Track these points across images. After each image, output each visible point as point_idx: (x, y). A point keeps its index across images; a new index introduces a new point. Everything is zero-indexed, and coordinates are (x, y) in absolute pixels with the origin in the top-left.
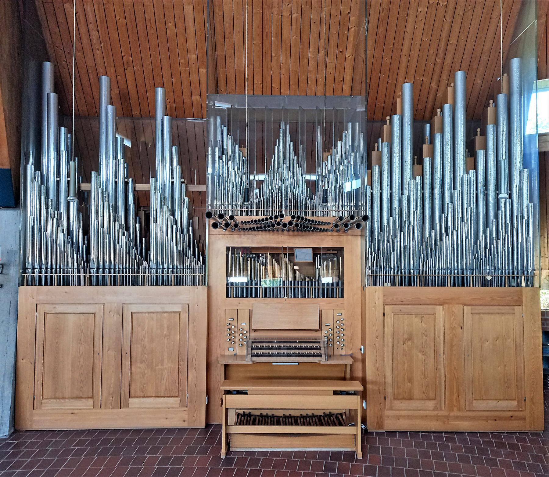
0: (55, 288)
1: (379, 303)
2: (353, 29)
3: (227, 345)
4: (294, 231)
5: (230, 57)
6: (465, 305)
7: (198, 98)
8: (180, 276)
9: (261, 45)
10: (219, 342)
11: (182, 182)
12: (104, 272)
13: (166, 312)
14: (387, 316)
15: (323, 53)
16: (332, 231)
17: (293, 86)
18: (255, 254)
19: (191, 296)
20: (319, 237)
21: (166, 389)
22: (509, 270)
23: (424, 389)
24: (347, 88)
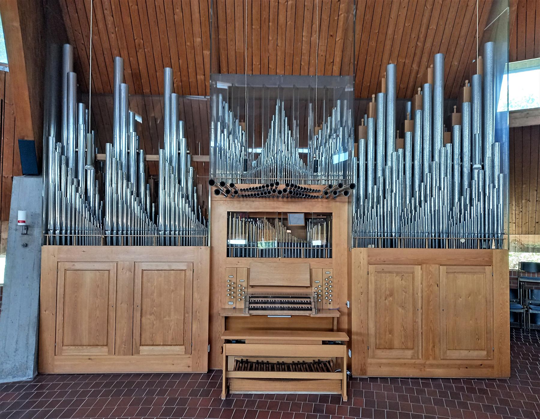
0: (121, 248)
2: (342, 15)
4: (288, 197)
5: (231, 40)
6: (441, 265)
7: (202, 77)
13: (173, 270)
15: (315, 36)
16: (322, 197)
17: (288, 67)
18: (253, 218)
19: (196, 255)
20: (311, 203)
21: (173, 339)
22: (481, 233)
23: (403, 340)
24: (336, 69)
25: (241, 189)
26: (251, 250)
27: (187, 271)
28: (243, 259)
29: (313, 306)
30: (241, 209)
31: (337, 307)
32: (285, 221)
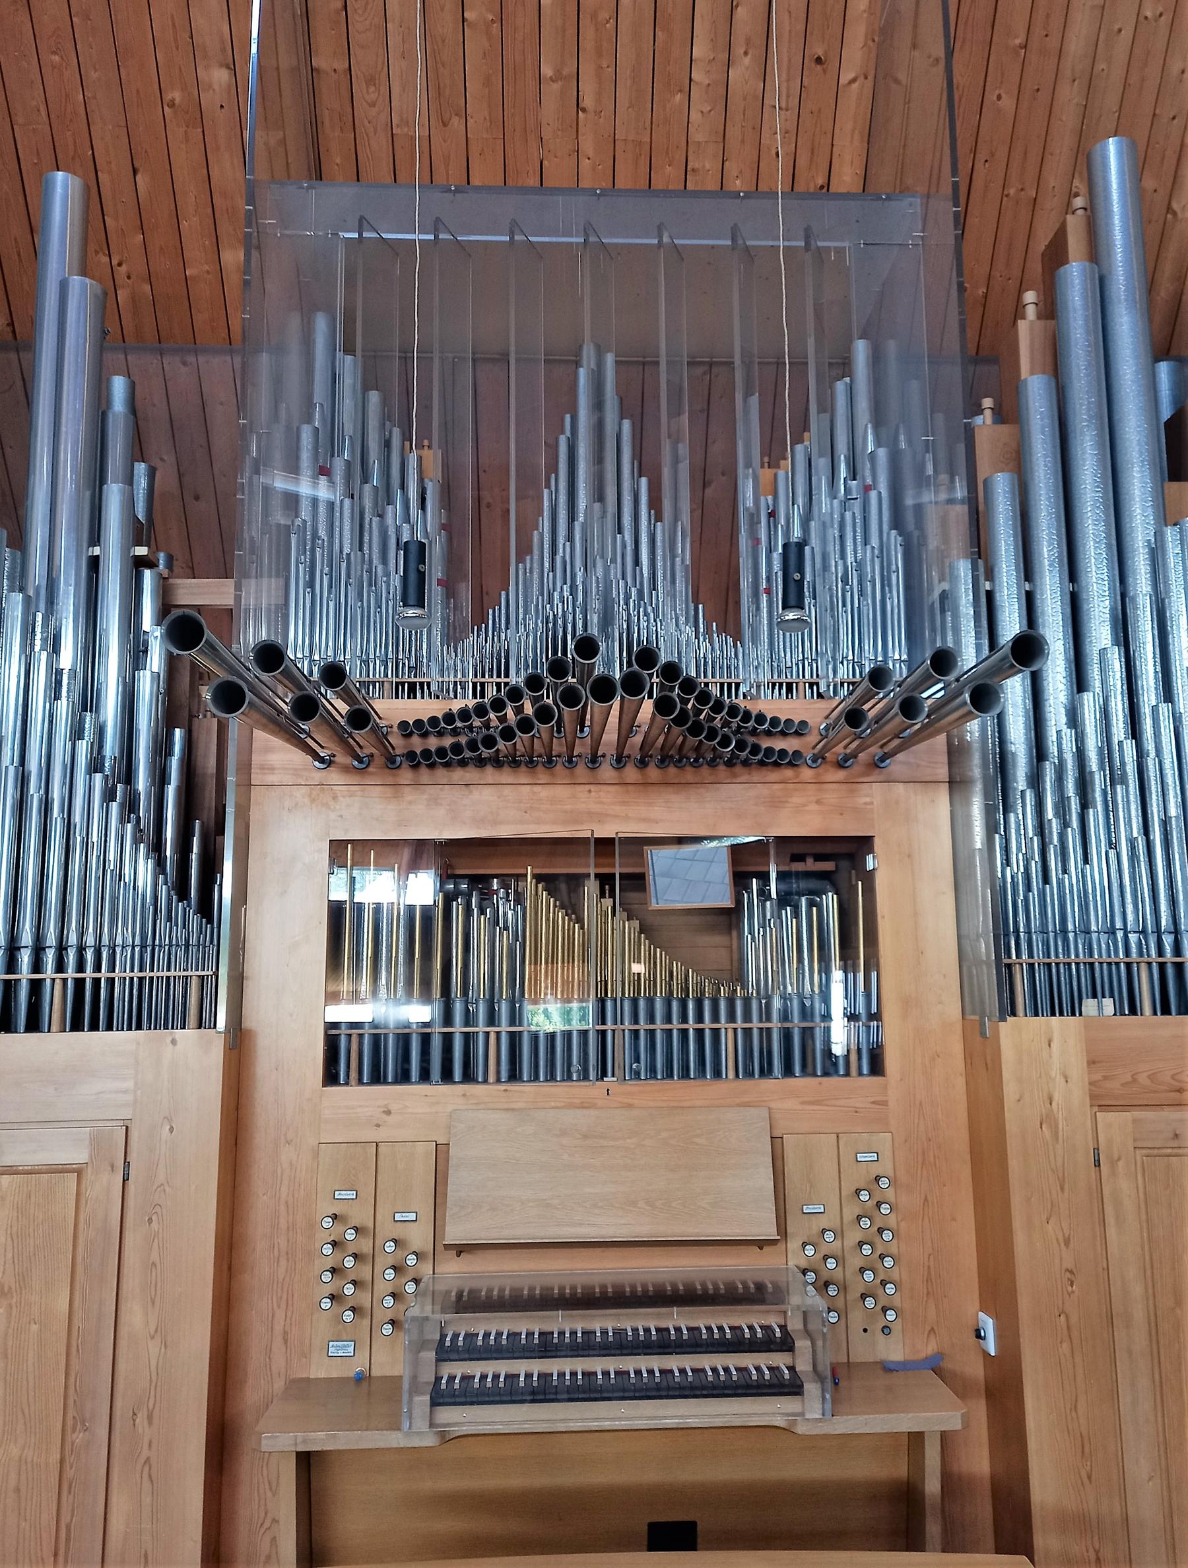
1: (1070, 1094)
3: (322, 1325)
4: (643, 764)
5: (371, 81)
8: (96, 982)
9: (496, 26)
10: (280, 1315)
11: (140, 563)
12: (37, 966)
14: (1113, 1163)
15: (742, 72)
16: (819, 758)
18: (475, 880)
19: (151, 1076)
25: (403, 725)
26: (707, 1033)
27: (89, 1175)
28: (415, 1091)
29: (803, 1366)
30: (401, 823)
31: (928, 1349)
32: (633, 896)
